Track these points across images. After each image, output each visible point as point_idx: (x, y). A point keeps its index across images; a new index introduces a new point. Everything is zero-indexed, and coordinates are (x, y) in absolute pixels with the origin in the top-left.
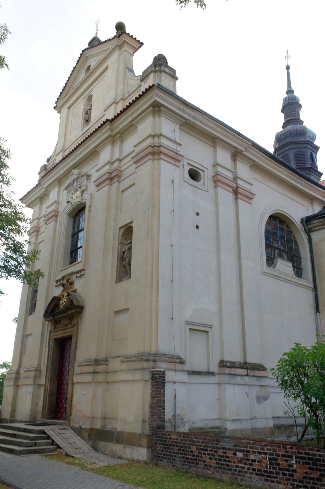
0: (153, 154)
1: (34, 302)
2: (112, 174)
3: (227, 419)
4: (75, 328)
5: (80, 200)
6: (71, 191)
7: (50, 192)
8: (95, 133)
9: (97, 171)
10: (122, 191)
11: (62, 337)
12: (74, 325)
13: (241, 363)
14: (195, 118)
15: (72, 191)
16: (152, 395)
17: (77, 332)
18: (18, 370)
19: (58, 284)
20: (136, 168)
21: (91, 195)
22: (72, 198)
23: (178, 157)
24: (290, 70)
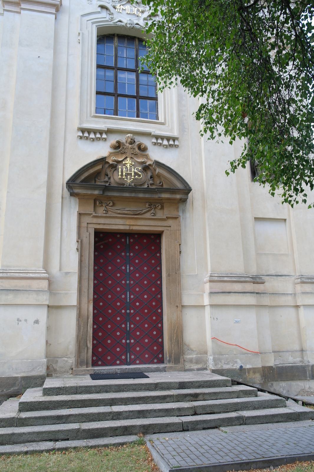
4: (170, 222)
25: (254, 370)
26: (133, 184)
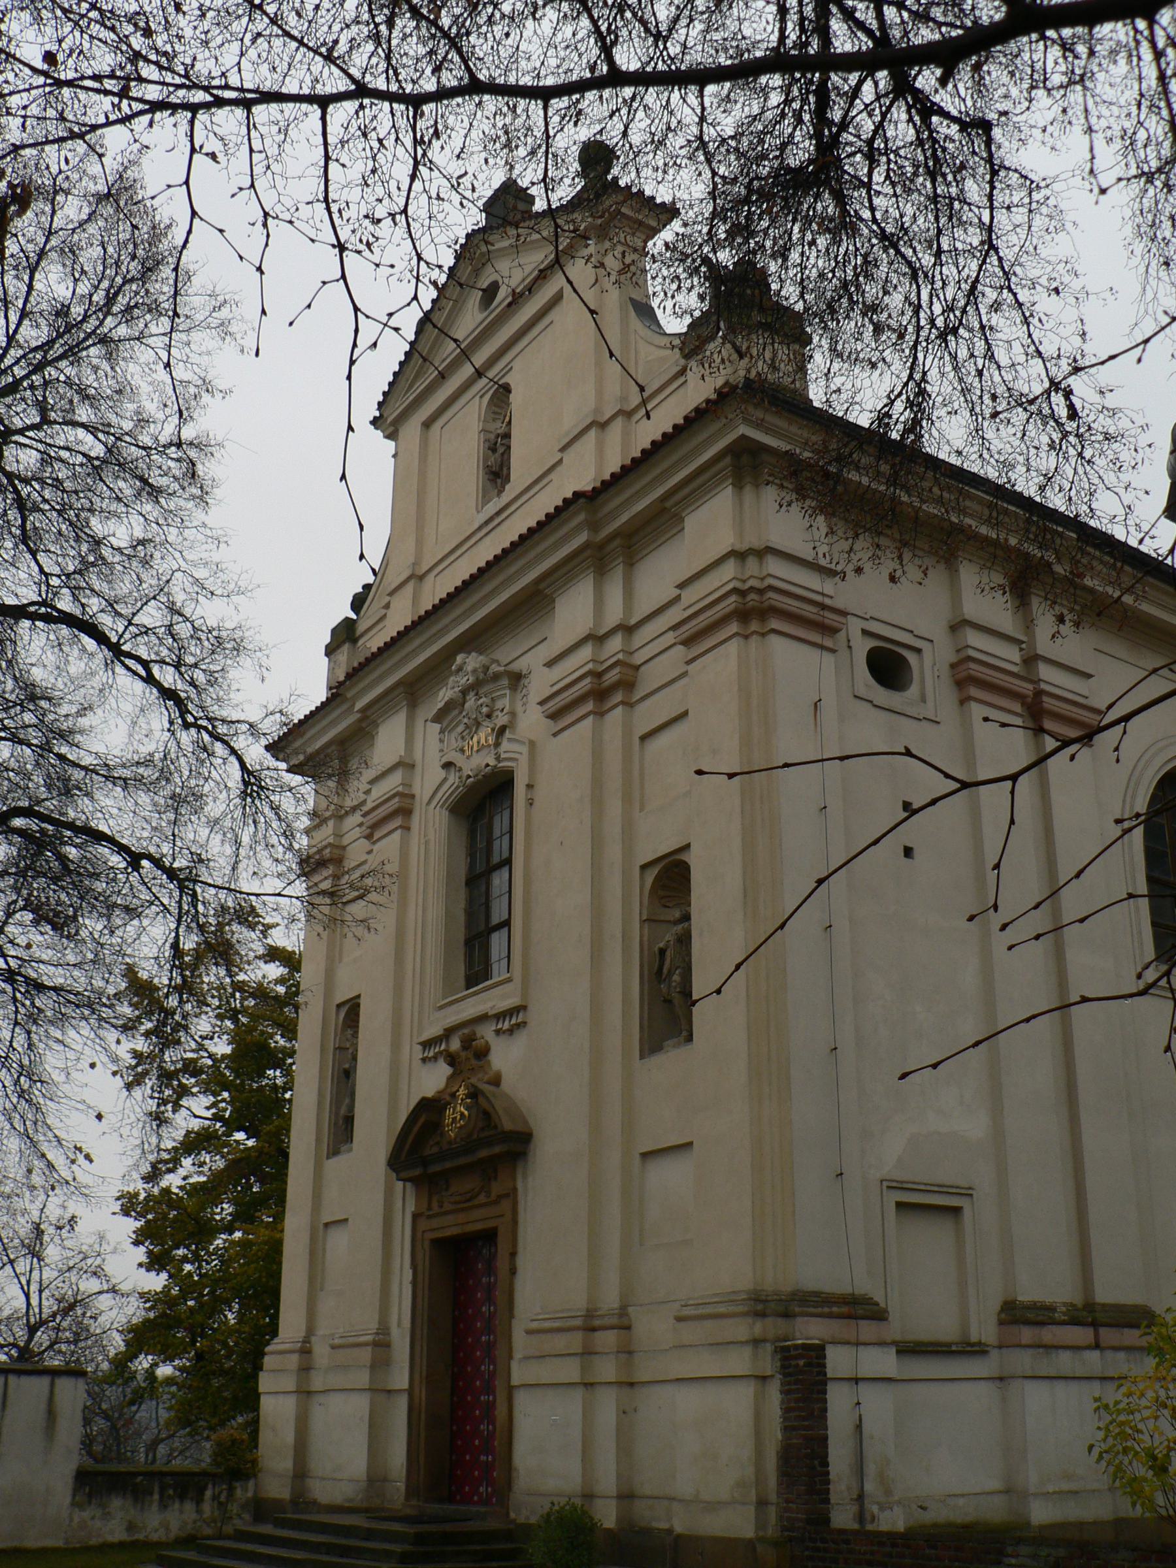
0: (743, 615)
1: (343, 1111)
2: (607, 676)
3: (1032, 1490)
4: (505, 1205)
5: (492, 762)
6: (457, 725)
7: (375, 725)
8: (536, 537)
9: (550, 664)
10: (643, 738)
12: (500, 1197)
13: (1072, 1305)
15: (461, 728)
17: (515, 1222)
18: (306, 1340)
19: (431, 1054)
20: (689, 662)
21: (532, 744)
22: (462, 751)
23: (830, 618)
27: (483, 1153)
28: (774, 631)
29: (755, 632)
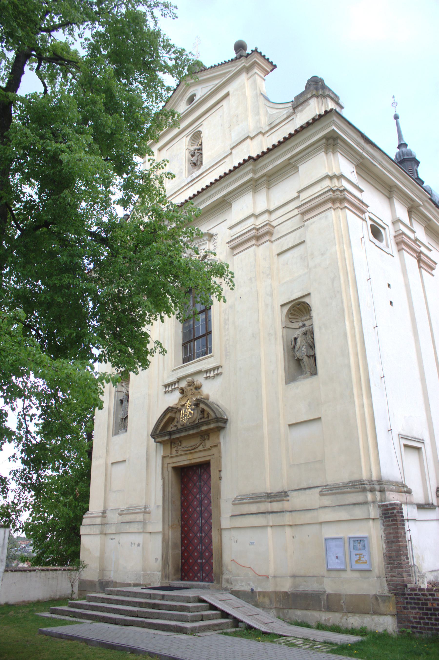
0: (333, 201)
4: (214, 450)
9: (231, 228)
11: (187, 464)
14: (373, 157)
16: (387, 539)
24: (400, 120)
25: (264, 594)
26: (188, 424)
27: (204, 428)
28: (346, 207)
29: (338, 207)
